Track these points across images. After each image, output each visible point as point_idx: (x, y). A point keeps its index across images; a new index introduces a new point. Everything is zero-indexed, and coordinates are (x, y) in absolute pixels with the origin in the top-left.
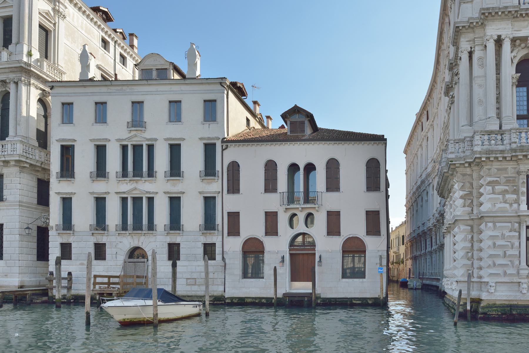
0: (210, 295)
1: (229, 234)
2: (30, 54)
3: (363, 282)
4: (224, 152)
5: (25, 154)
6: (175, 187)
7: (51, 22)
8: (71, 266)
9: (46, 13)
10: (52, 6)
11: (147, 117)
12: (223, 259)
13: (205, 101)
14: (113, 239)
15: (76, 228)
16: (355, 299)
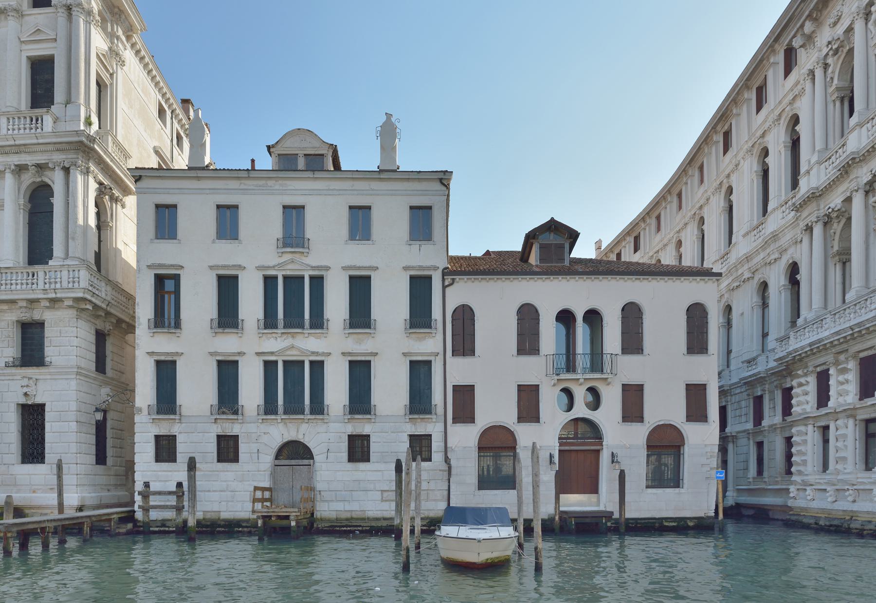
0: (423, 516)
1: (456, 420)
2: (89, 123)
3: (679, 493)
4: (448, 290)
5: (90, 288)
6: (360, 345)
7: (107, 70)
8: (176, 473)
9: (103, 55)
10: (109, 45)
11: (310, 232)
12: (447, 460)
13: (411, 208)
14: (252, 428)
15: (184, 411)
16: (666, 519)
